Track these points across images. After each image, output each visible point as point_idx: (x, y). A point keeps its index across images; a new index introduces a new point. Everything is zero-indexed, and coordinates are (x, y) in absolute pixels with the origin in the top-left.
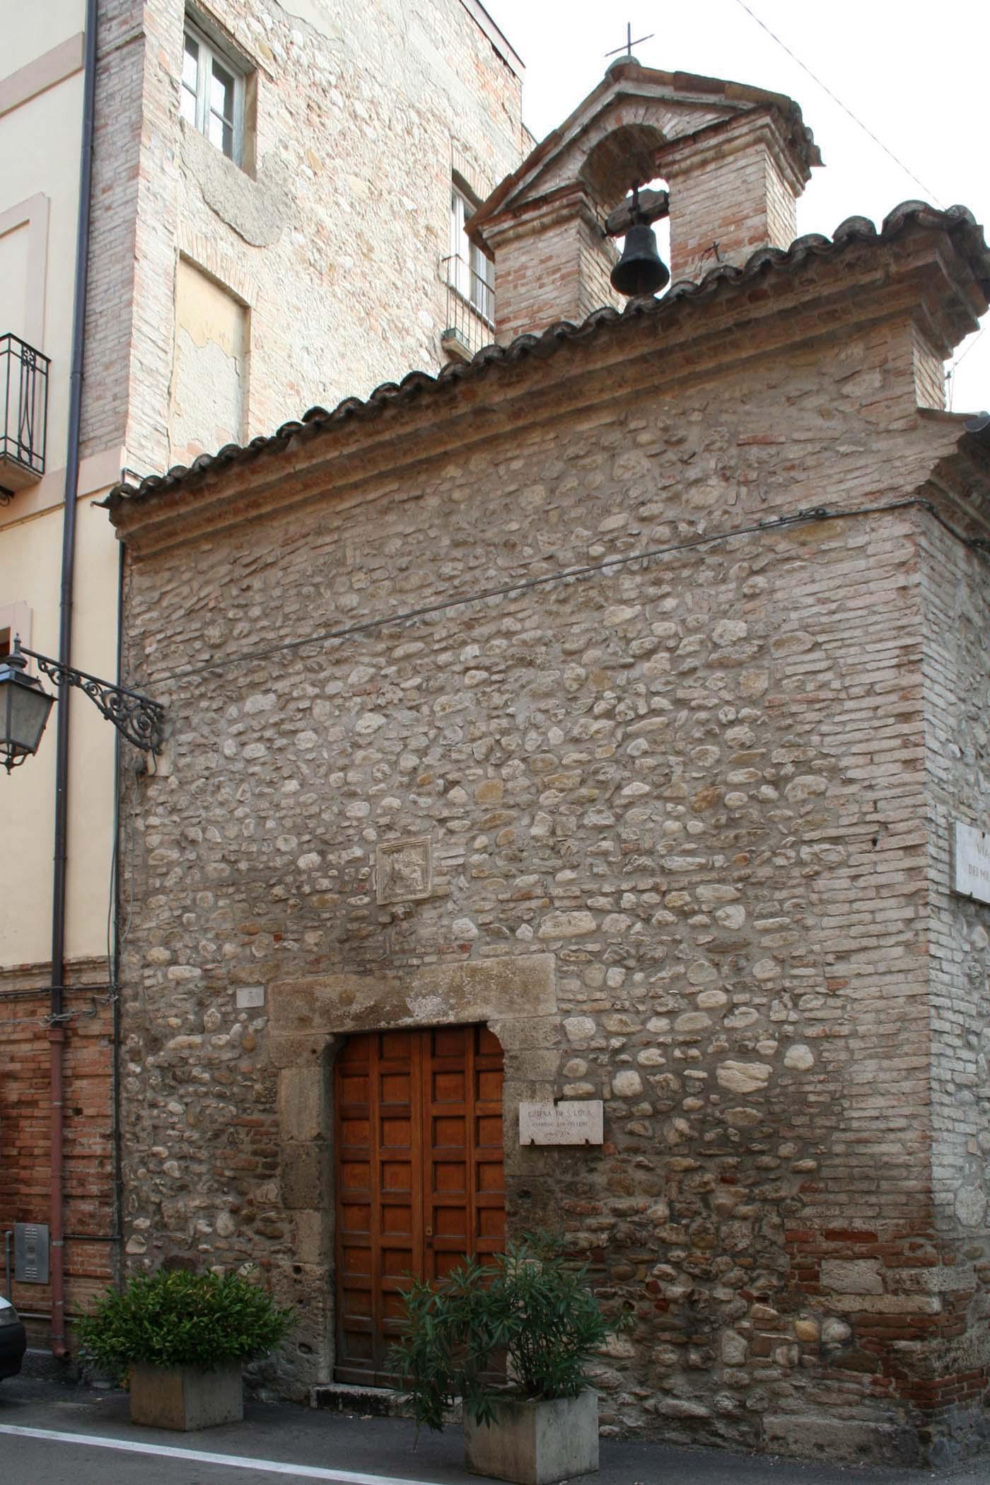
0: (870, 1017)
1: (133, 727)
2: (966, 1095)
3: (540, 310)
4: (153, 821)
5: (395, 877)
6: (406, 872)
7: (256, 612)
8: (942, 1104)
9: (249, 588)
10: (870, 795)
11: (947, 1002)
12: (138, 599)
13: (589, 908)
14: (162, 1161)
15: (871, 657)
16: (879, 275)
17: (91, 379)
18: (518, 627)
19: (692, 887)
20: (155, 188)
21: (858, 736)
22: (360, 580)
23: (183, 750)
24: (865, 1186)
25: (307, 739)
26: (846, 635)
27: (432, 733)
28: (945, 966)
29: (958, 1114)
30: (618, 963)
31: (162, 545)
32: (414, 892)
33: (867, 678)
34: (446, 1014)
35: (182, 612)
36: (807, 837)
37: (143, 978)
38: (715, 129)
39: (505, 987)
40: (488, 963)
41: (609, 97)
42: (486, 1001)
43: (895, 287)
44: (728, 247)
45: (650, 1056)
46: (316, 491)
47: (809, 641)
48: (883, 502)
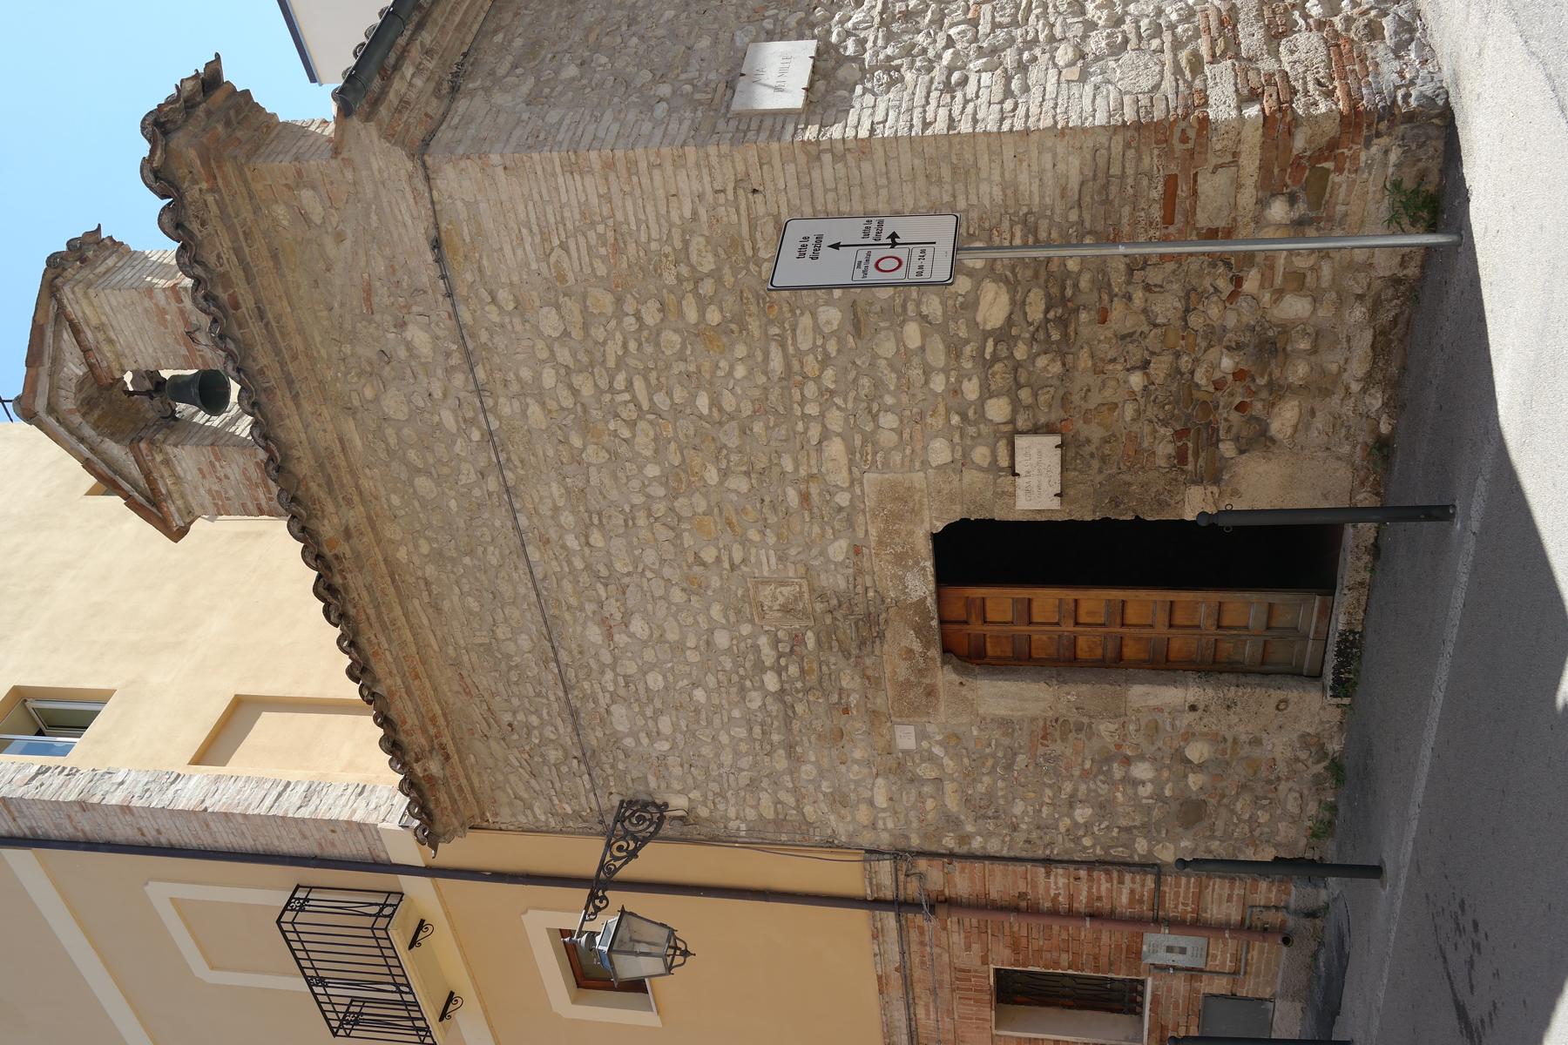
0: (934, 191)
1: (644, 829)
2: (1015, 85)
3: (248, 479)
4: (732, 813)
5: (786, 610)
6: (781, 600)
7: (534, 720)
8: (1027, 116)
9: (510, 725)
10: (710, 197)
11: (917, 113)
12: (522, 819)
13: (820, 442)
14: (1076, 824)
15: (573, 197)
16: (210, 198)
17: (316, 851)
18: (549, 501)
19: (800, 355)
20: (138, 791)
21: (650, 208)
22: (502, 632)
23: (663, 785)
24: (1114, 189)
25: (655, 681)
26: (552, 220)
27: (649, 575)
28: (879, 117)
29: (1036, 92)
30: (875, 417)
31: (470, 797)
32: (801, 593)
33: (594, 201)
34: (924, 568)
35: (533, 782)
36: (750, 253)
37: (885, 829)
38: (76, 331)
39: (897, 517)
40: (873, 532)
41: (51, 421)
42: (911, 533)
43: (220, 181)
44: (187, 322)
45: (971, 390)
46: (420, 669)
47: (558, 252)
48: (421, 185)
